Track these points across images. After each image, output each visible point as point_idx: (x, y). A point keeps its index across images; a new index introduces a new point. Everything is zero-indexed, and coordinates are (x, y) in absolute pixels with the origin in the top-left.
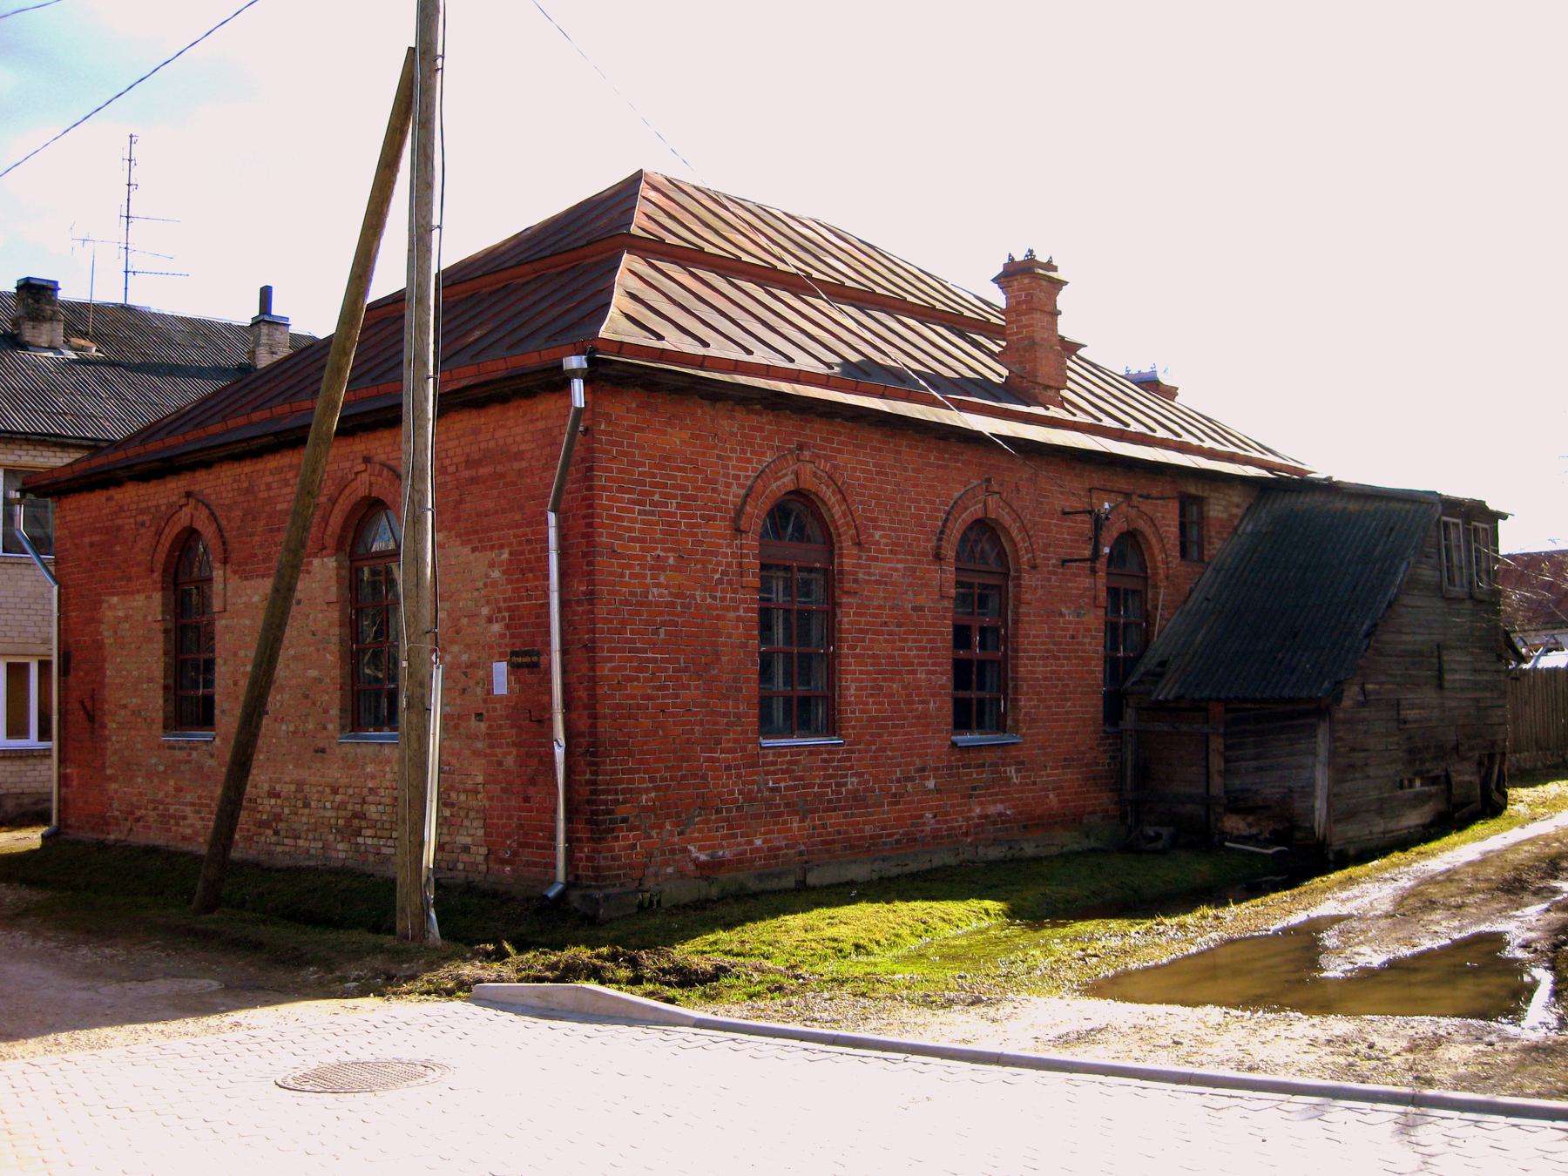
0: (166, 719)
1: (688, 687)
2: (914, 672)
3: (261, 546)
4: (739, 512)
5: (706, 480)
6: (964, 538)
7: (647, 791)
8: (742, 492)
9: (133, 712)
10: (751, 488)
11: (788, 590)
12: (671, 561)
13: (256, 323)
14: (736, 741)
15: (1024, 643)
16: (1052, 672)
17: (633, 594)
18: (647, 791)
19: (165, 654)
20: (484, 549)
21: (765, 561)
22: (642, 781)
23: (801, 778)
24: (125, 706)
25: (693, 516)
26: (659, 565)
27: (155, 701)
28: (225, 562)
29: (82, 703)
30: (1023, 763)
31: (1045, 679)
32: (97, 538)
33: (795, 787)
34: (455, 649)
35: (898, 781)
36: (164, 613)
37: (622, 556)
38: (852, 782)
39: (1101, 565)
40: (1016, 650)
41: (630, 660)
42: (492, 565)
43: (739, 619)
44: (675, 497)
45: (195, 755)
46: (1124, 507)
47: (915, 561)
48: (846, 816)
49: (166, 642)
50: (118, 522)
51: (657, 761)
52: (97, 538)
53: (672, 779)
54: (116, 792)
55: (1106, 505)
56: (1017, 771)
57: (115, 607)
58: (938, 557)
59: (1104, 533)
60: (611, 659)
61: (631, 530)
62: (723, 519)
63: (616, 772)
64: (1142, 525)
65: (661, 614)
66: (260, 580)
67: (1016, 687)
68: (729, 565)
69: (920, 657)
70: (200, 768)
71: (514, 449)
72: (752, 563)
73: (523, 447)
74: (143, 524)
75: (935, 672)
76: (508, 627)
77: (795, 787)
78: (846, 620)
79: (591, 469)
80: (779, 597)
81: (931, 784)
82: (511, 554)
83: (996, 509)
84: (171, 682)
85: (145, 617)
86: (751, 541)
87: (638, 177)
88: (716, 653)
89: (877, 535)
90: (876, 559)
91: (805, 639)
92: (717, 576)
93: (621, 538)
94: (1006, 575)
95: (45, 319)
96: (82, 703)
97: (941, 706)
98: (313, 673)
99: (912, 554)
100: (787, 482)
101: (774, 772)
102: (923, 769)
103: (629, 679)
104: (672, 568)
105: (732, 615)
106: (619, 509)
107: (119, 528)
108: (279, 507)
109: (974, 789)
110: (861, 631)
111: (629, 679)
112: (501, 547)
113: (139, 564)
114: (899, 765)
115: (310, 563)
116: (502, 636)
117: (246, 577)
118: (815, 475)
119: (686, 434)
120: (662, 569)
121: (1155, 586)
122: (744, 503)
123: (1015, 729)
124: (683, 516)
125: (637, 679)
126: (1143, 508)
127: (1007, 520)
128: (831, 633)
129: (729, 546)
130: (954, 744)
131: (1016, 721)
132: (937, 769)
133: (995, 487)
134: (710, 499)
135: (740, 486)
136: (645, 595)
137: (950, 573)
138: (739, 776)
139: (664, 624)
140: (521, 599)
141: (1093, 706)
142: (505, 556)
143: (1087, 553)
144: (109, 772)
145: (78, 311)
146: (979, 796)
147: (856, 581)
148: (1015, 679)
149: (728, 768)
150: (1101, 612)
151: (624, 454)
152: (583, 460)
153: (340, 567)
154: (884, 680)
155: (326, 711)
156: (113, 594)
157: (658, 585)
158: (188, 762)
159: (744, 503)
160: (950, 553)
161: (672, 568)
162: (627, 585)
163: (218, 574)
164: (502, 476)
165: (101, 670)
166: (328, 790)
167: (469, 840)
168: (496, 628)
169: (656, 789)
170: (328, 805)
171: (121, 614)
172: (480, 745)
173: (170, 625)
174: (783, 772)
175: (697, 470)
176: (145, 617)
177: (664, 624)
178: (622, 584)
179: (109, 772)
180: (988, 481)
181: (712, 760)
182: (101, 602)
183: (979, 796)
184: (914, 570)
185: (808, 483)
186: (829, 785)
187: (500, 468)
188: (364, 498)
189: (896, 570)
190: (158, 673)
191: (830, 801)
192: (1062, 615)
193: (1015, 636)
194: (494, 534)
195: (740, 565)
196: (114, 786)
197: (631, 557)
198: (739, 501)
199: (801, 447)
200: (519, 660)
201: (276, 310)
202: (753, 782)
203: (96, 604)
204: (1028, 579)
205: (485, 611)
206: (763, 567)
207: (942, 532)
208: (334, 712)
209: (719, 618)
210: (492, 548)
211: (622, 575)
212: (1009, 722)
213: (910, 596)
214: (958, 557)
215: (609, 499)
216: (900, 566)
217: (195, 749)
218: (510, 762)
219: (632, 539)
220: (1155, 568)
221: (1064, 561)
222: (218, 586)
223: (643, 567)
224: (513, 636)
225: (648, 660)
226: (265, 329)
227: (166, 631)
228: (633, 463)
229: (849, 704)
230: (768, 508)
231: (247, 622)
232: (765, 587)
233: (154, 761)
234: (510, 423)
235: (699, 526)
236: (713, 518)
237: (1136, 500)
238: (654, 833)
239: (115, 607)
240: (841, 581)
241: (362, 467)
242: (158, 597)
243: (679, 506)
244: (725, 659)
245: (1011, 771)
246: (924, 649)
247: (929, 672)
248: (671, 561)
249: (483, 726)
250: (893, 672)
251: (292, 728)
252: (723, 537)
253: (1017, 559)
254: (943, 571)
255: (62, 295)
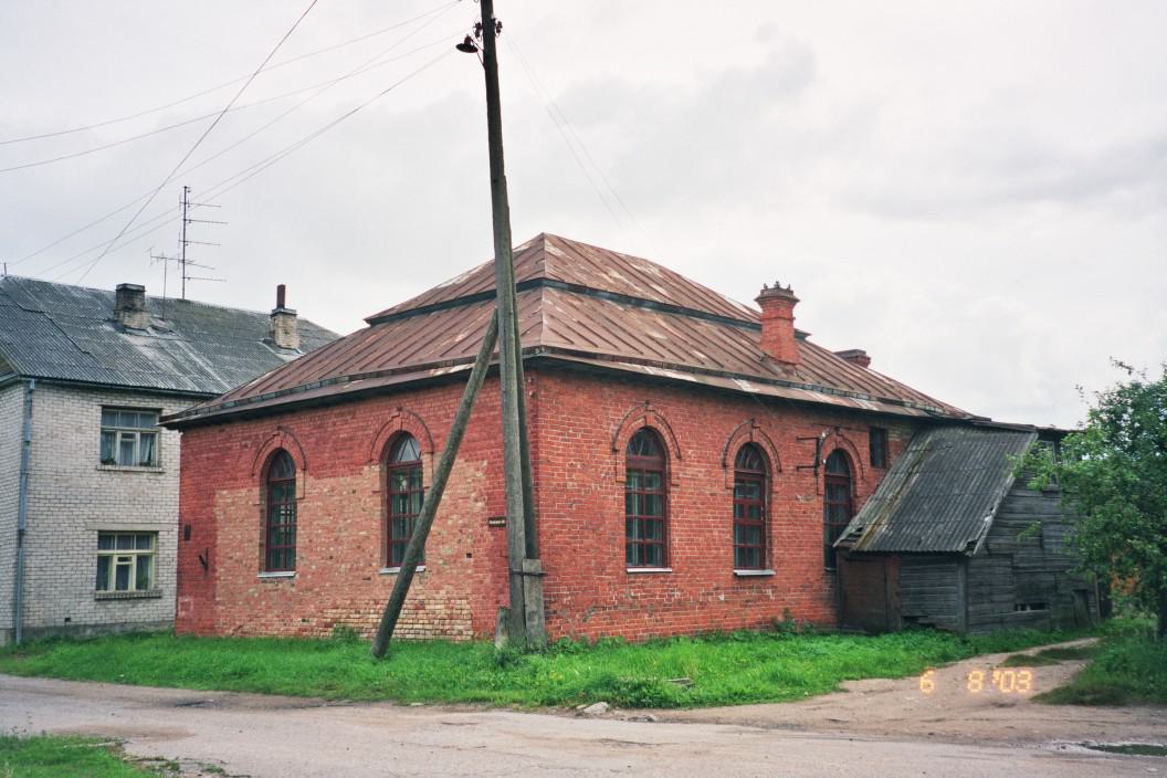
0: (260, 564)
1: (587, 538)
2: (711, 531)
3: (329, 459)
4: (615, 440)
5: (597, 421)
6: (739, 454)
7: (567, 595)
8: (616, 428)
9: (237, 561)
10: (621, 426)
11: (641, 485)
12: (579, 467)
13: (274, 314)
14: (613, 568)
15: (775, 515)
16: (792, 533)
17: (558, 485)
18: (567, 595)
19: (261, 525)
20: (473, 460)
21: (632, 465)
22: (564, 590)
23: (649, 591)
24: (231, 558)
25: (590, 442)
26: (572, 470)
27: (254, 553)
28: (304, 470)
29: (200, 557)
30: (776, 587)
31: (789, 537)
32: (212, 455)
33: (645, 597)
34: (455, 517)
35: (703, 594)
36: (261, 500)
37: (552, 464)
38: (677, 594)
39: (821, 470)
40: (771, 520)
41: (557, 522)
42: (478, 470)
43: (615, 499)
44: (580, 431)
45: (280, 586)
46: (834, 436)
47: (712, 467)
48: (674, 614)
49: (261, 518)
50: (228, 445)
51: (572, 578)
52: (212, 455)
53: (580, 589)
54: (222, 611)
55: (824, 435)
56: (773, 592)
57: (224, 497)
58: (725, 466)
59: (822, 450)
60: (547, 521)
61: (558, 449)
62: (606, 443)
63: (550, 585)
64: (845, 446)
65: (574, 496)
66: (328, 480)
67: (771, 542)
68: (609, 469)
69: (714, 522)
70: (284, 593)
71: (490, 404)
72: (622, 468)
73: (496, 403)
74: (246, 446)
75: (723, 532)
76: (487, 504)
77: (645, 597)
78: (674, 500)
79: (536, 416)
80: (635, 487)
81: (722, 598)
82: (489, 463)
83: (757, 438)
84: (264, 541)
85: (247, 503)
86: (622, 457)
87: (542, 238)
88: (603, 519)
89: (690, 452)
90: (690, 466)
91: (650, 512)
92: (603, 475)
93: (551, 454)
94: (763, 476)
95: (136, 311)
96: (200, 557)
97: (727, 552)
98: (363, 533)
99: (709, 463)
100: (640, 423)
101: (634, 588)
102: (717, 589)
103: (557, 533)
104: (580, 471)
105: (610, 497)
106: (551, 438)
107: (230, 449)
108: (341, 436)
109: (747, 601)
110: (681, 507)
111: (557, 533)
112: (483, 459)
113: (242, 471)
114: (702, 585)
115: (362, 469)
116: (483, 509)
117: (318, 477)
118: (656, 418)
119: (586, 397)
120: (574, 471)
121: (855, 483)
122: (617, 434)
123: (771, 567)
124: (586, 442)
125: (561, 532)
126: (846, 436)
127: (764, 444)
128: (665, 511)
129: (610, 458)
130: (735, 574)
131: (771, 562)
132: (726, 588)
133: (757, 425)
134: (598, 432)
135: (615, 425)
136: (565, 485)
137: (731, 475)
138: (615, 589)
139: (575, 502)
140: (494, 488)
141: (818, 554)
142: (485, 463)
143: (812, 463)
144: (218, 599)
145: (162, 304)
146: (750, 606)
147: (678, 478)
148: (770, 537)
149: (609, 584)
150: (821, 498)
151: (553, 407)
152: (532, 411)
153: (381, 471)
154: (695, 535)
155: (372, 556)
156: (224, 489)
157: (572, 480)
158: (277, 590)
159: (617, 434)
160: (731, 462)
161: (580, 471)
162: (557, 480)
163: (299, 475)
164: (483, 419)
165: (215, 537)
166: (372, 602)
167: (461, 627)
168: (480, 504)
169: (571, 595)
170: (372, 611)
171: (229, 501)
172: (470, 571)
173: (265, 508)
174: (639, 587)
175: (592, 416)
176: (247, 503)
177: (575, 502)
178: (553, 479)
179: (218, 599)
180: (753, 420)
181: (601, 579)
182: (215, 494)
183: (750, 606)
184: (711, 472)
185: (653, 423)
186: (664, 596)
187: (482, 415)
188: (397, 432)
189: (700, 472)
190: (256, 536)
191: (665, 605)
192: (797, 499)
193: (770, 511)
194: (479, 452)
195: (615, 469)
196: (221, 608)
197: (559, 465)
198: (614, 433)
199: (648, 403)
200: (494, 522)
201: (288, 305)
202: (623, 592)
203: (211, 495)
204: (777, 478)
205: (473, 495)
206: (628, 470)
207: (726, 451)
208: (377, 556)
209: (604, 498)
210: (477, 460)
211: (553, 475)
212: (767, 563)
213: (708, 487)
214: (736, 465)
215: (546, 432)
216: (703, 470)
217: (282, 582)
218: (487, 581)
219: (558, 455)
220: (855, 472)
221: (798, 467)
222: (299, 483)
223: (564, 470)
224: (490, 509)
225: (567, 522)
226: (281, 318)
227: (262, 511)
228: (557, 413)
229: (675, 549)
230: (630, 436)
231: (320, 504)
232: (628, 482)
233: (251, 590)
234: (489, 389)
235: (592, 447)
236: (601, 443)
237: (842, 431)
238: (570, 620)
239: (224, 497)
240: (670, 478)
241: (397, 414)
242: (256, 491)
243: (583, 436)
244: (607, 522)
245: (769, 592)
246: (716, 518)
247: (719, 532)
248: (579, 467)
249: (472, 560)
250: (700, 531)
251: (349, 566)
252: (606, 453)
253: (770, 466)
254: (727, 473)
255: (149, 293)
